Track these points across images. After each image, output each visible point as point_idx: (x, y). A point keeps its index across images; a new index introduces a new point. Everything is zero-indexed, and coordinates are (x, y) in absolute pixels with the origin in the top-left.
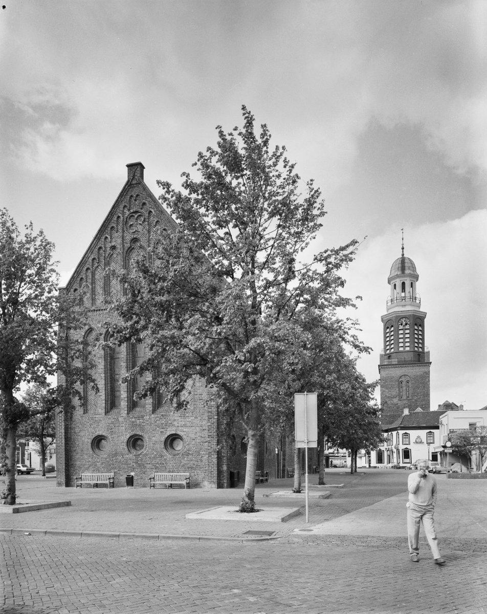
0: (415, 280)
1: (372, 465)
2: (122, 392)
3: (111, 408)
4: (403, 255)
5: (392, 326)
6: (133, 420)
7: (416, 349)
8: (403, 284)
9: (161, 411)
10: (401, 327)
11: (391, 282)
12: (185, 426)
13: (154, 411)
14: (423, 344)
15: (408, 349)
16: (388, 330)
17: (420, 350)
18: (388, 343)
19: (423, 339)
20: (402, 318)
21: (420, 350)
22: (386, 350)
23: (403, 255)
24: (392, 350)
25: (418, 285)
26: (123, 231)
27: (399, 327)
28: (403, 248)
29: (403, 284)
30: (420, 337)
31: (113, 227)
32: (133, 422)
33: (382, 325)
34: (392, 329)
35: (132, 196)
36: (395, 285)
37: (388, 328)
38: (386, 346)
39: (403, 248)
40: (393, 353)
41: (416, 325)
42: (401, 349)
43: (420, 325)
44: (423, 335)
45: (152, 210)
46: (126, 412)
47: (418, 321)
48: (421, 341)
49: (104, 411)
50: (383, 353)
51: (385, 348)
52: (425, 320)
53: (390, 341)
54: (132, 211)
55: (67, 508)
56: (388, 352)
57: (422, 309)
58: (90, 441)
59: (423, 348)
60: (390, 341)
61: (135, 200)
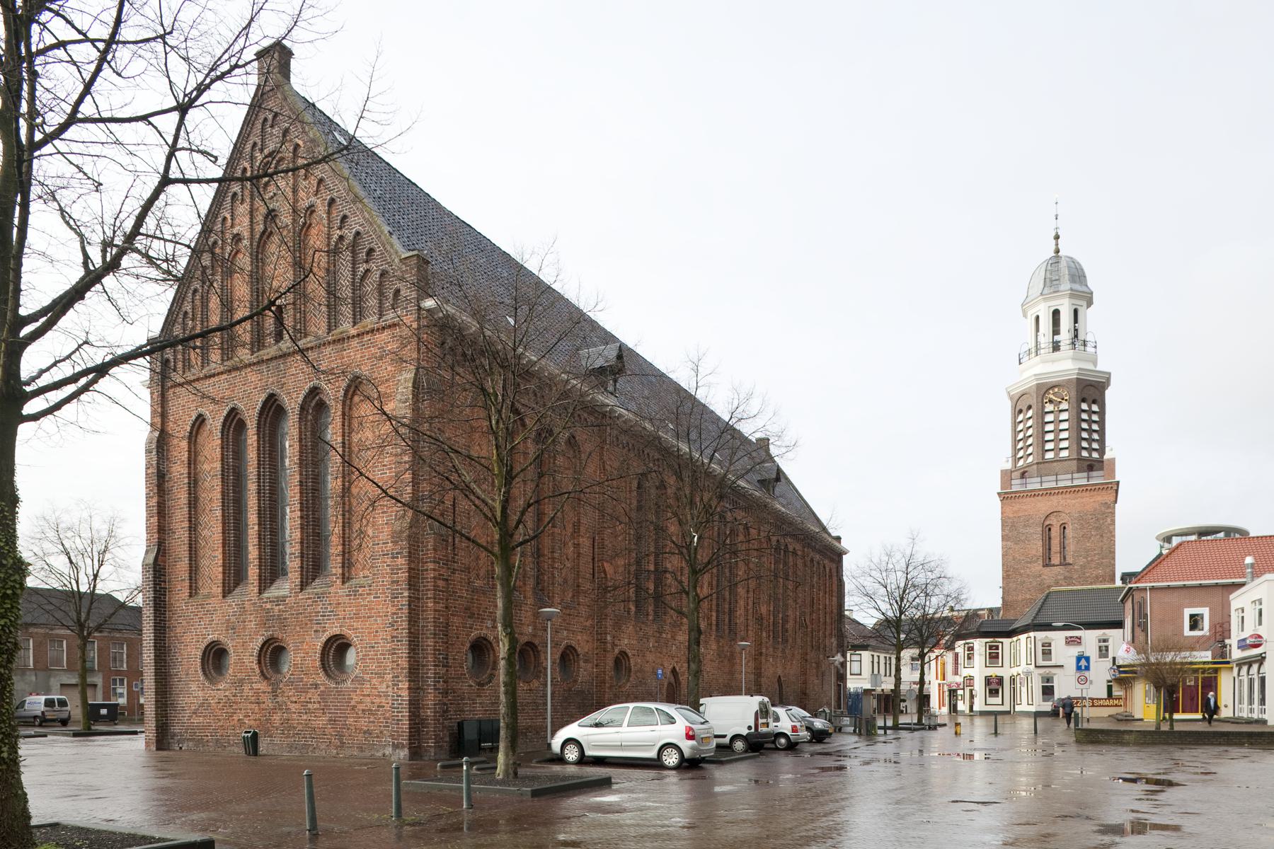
0: (1085, 304)
1: (975, 708)
2: (250, 548)
3: (237, 584)
4: (1057, 251)
5: (1030, 407)
6: (269, 606)
7: (1085, 454)
8: (1056, 313)
9: (317, 586)
10: (1049, 407)
11: (1029, 314)
12: (357, 616)
13: (303, 586)
14: (1102, 441)
15: (1064, 454)
16: (1021, 417)
17: (1095, 455)
18: (1021, 445)
19: (1102, 432)
20: (1053, 387)
21: (1095, 455)
22: (1016, 460)
23: (1057, 251)
24: (1030, 459)
25: (1091, 318)
26: (252, 199)
27: (1043, 407)
28: (1057, 237)
29: (1056, 313)
30: (1096, 436)
31: (235, 194)
32: (268, 611)
33: (1008, 406)
34: (1030, 413)
35: (266, 120)
36: (1037, 318)
37: (1021, 411)
38: (1016, 451)
39: (1057, 237)
40: (1030, 465)
41: (1084, 400)
42: (1050, 455)
43: (1094, 402)
44: (1102, 423)
45: (300, 143)
46: (256, 590)
47: (1091, 391)
48: (1096, 436)
49: (220, 590)
50: (1009, 466)
51: (1015, 455)
52: (1107, 392)
53: (1026, 438)
54: (266, 152)
55: (1174, 834)
56: (1021, 463)
57: (1101, 367)
58: (200, 653)
59: (1102, 451)
60: (1026, 438)
61: (272, 126)
